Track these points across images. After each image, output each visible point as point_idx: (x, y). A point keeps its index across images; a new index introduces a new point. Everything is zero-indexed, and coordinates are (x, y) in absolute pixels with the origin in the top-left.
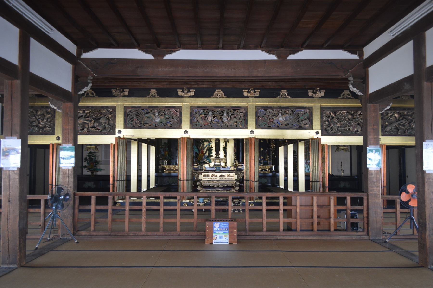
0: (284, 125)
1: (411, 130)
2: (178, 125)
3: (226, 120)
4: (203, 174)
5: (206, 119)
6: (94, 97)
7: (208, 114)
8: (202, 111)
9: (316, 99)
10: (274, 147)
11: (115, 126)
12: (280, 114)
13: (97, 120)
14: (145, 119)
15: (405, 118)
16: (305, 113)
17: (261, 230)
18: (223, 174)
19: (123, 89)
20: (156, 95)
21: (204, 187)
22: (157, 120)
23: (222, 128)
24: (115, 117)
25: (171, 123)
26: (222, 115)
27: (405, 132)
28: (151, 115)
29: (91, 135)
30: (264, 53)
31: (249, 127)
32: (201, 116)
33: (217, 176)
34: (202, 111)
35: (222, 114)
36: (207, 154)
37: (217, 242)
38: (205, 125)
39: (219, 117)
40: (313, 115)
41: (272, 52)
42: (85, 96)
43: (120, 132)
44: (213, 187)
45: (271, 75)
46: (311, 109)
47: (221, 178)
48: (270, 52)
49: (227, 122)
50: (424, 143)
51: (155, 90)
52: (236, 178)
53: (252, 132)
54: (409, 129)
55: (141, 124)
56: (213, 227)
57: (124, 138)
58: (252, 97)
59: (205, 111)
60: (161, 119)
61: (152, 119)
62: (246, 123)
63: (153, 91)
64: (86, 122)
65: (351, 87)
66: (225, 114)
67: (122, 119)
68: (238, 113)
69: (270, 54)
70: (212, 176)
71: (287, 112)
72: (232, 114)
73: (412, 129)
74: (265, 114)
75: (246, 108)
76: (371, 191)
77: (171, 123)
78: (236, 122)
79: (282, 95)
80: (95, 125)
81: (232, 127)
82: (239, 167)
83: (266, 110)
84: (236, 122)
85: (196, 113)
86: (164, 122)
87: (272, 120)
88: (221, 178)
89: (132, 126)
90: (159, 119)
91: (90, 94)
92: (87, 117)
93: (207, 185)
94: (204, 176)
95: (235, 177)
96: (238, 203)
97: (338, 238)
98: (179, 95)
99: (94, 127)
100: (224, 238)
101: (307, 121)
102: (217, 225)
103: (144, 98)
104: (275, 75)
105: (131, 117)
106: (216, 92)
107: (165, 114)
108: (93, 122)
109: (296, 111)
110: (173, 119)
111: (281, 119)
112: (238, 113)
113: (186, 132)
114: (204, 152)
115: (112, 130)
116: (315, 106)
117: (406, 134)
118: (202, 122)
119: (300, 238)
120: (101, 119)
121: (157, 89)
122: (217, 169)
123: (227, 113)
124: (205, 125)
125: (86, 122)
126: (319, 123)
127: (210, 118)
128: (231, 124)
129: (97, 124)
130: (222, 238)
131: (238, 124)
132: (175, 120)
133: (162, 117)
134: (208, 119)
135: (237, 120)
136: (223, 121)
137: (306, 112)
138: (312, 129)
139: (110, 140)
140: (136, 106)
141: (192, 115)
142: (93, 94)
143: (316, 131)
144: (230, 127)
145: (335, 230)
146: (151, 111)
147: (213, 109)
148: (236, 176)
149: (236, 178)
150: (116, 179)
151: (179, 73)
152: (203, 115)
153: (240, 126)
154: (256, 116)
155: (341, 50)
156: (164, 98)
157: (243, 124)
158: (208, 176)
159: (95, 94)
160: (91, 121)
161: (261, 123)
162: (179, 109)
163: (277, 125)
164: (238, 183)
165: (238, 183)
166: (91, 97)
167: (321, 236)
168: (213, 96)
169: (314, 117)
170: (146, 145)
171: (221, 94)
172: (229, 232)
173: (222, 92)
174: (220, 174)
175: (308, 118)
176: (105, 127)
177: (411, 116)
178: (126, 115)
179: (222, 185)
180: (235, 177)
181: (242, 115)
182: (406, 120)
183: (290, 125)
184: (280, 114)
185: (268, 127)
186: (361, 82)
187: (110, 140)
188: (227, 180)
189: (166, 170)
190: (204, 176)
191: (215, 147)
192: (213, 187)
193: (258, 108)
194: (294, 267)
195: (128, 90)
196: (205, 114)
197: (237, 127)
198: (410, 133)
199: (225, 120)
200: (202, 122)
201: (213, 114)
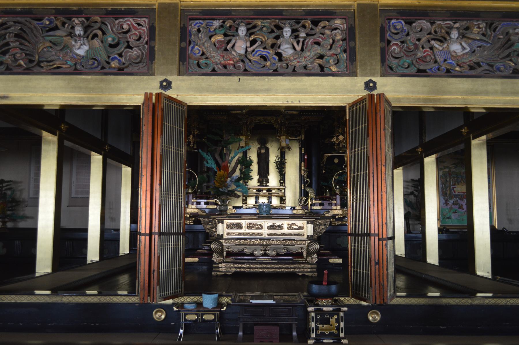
2: (145, 65)
3: (291, 51)
4: (227, 221)
5: (229, 47)
7: (236, 34)
8: (216, 24)
12: (454, 34)
18: (278, 223)
21: (229, 254)
22: (82, 50)
25: (123, 60)
26: (277, 38)
32: (213, 39)
33: (261, 227)
35: (277, 33)
36: (237, 173)
38: (225, 67)
39: (270, 41)
44: (252, 254)
49: (292, 55)
52: (311, 233)
55: (31, 61)
59: (228, 24)
61: (66, 47)
66: (287, 32)
72: (308, 35)
74: (408, 35)
77: (123, 60)
78: (321, 57)
82: (314, 208)
84: (321, 57)
85: (199, 31)
86: (103, 57)
87: (429, 52)
90: (86, 48)
93: (235, 249)
94: (229, 227)
95: (309, 229)
96: (332, 314)
107: (104, 33)
110: (129, 47)
111: (456, 48)
112: (328, 32)
114: (230, 169)
118: (216, 57)
122: (265, 213)
123: (294, 31)
124: (225, 67)
127: (241, 46)
128: (304, 63)
132: (135, 52)
133: (96, 42)
134: (236, 48)
136: (279, 55)
144: (304, 71)
146: (64, 24)
148: (311, 226)
149: (311, 233)
152: (220, 38)
153: (334, 69)
158: (240, 226)
163: (444, 67)
164: (317, 246)
165: (317, 246)
170: (100, 157)
174: (270, 222)
179: (274, 250)
180: (309, 229)
181: (339, 37)
184: (454, 34)
185: (419, 71)
188: (288, 239)
190: (229, 227)
191: (259, 163)
192: (252, 254)
196: (225, 35)
199: (286, 50)
200: (216, 57)
201: (251, 34)
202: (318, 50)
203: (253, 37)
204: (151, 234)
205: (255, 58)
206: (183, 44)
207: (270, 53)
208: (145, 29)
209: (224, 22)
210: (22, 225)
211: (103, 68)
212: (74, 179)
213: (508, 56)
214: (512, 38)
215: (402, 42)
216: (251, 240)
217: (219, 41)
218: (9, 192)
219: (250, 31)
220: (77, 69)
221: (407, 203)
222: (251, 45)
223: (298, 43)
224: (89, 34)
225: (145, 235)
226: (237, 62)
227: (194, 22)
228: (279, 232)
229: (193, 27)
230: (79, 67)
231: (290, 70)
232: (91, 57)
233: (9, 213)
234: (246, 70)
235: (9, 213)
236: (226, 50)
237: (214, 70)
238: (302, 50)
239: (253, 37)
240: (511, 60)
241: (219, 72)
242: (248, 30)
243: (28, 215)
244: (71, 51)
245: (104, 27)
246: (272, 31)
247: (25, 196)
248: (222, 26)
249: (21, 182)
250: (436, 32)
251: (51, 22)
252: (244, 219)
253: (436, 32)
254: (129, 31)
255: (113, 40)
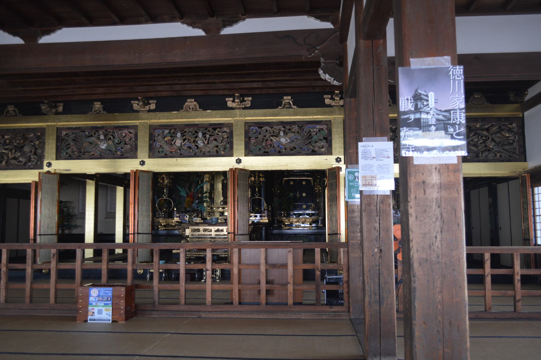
0: (288, 150)
1: (487, 153)
2: (132, 154)
3: (202, 144)
6: (16, 115)
8: (167, 131)
9: (336, 108)
10: (319, 190)
11: (44, 156)
12: (282, 134)
13: (20, 148)
14: (86, 145)
15: (479, 135)
16: (320, 130)
17: (178, 304)
19: (56, 102)
20: (102, 110)
22: (103, 146)
23: (195, 156)
24: (44, 143)
25: (123, 150)
26: (196, 137)
27: (477, 156)
28: (93, 139)
29: (11, 169)
30: (185, 26)
31: (234, 155)
32: (166, 139)
34: (167, 131)
37: (94, 320)
38: (171, 152)
39: (192, 140)
40: (333, 133)
41: (197, 25)
42: (5, 114)
43: (49, 165)
45: (195, 59)
46: (328, 123)
47: (218, 233)
48: (193, 24)
50: (360, 144)
51: (99, 103)
53: (239, 161)
54: (485, 150)
55: (80, 152)
56: (88, 296)
57: (55, 174)
58: (239, 108)
59: (172, 131)
60: (108, 145)
61: (96, 145)
62: (231, 148)
63: (98, 105)
64: (4, 151)
65: (321, 72)
66: (200, 135)
67: (54, 146)
68: (220, 134)
69: (194, 27)
70: (205, 230)
71: (294, 130)
72: (210, 135)
73: (489, 150)
74: (260, 134)
75: (230, 126)
76: (352, 240)
78: (217, 146)
79: (285, 105)
80: (17, 156)
81: (211, 154)
83: (261, 128)
84: (217, 146)
86: (113, 149)
88: (218, 233)
89: (67, 156)
90: (105, 145)
91: (11, 112)
92: (7, 145)
97: (299, 316)
98: (135, 109)
99: (15, 158)
100: (104, 313)
101: (323, 143)
102: (94, 292)
103: (83, 115)
104: (400, 101)
105: (67, 143)
106: (187, 104)
107: (114, 138)
108: (14, 151)
109: (306, 128)
110: (125, 144)
111: (283, 140)
112: (220, 134)
113: (143, 163)
115: (39, 163)
116: (334, 118)
117: (481, 158)
119: (237, 316)
120: (25, 147)
121: (103, 101)
124: (171, 152)
125: (4, 151)
126: (342, 145)
127: (178, 142)
129: (19, 154)
130: (101, 313)
131: (220, 149)
132: (128, 146)
133: (110, 142)
135: (218, 144)
137: (322, 129)
138: (332, 154)
139: (27, 177)
140: (74, 126)
141: (152, 138)
142: (14, 111)
143: (336, 157)
144: (208, 154)
145: (295, 304)
146: (95, 134)
147: (183, 129)
150: (38, 233)
151: (59, 64)
152: (169, 138)
154: (245, 137)
155: (305, 17)
156: (111, 114)
157: (227, 150)
159: (17, 111)
160: (11, 150)
161: (254, 148)
162: (134, 129)
163: (278, 149)
166: (13, 116)
167: (273, 312)
168: (182, 108)
169: (333, 136)
171: (195, 105)
172: (112, 304)
173: (195, 103)
175: (325, 138)
176: (31, 158)
177: (487, 130)
178: (60, 140)
181: (226, 136)
182: (478, 138)
183: (298, 149)
184: (282, 134)
185: (265, 152)
186: (337, 64)
187: (27, 177)
189: (161, 225)
193: (248, 125)
194: (140, 356)
195: (62, 104)
196: (171, 137)
197: (217, 154)
198: (486, 156)
199: (200, 144)
200: (167, 148)
201: (183, 136)
202: (215, 143)
203: (184, 137)
204: (134, 234)
205: (185, 148)
206: (151, 142)
207: (193, 145)
208: (132, 135)
209: (170, 130)
210: (75, 231)
211: (114, 154)
212: (109, 200)
213: (310, 142)
214: (312, 133)
215: (256, 138)
216: (205, 238)
217: (168, 140)
218: (65, 209)
219: (183, 135)
220: (101, 157)
221: (129, 226)
222: (184, 141)
223: (206, 140)
224: (107, 138)
225: (131, 234)
226: (177, 150)
227: (156, 131)
228: (197, 233)
229: (156, 133)
230: (102, 154)
231: (202, 153)
232: (108, 150)
233: (66, 223)
234: (181, 154)
235: (66, 223)
236: (171, 144)
237: (166, 154)
238: (208, 143)
239: (184, 137)
240: (311, 145)
241: (169, 155)
242: (182, 134)
243: (78, 225)
244: (99, 147)
245: (113, 134)
246: (194, 134)
247: (76, 211)
248: (169, 133)
249: (73, 202)
250: (274, 132)
251: (89, 133)
252: (201, 226)
253: (274, 132)
254: (126, 136)
255: (118, 141)
